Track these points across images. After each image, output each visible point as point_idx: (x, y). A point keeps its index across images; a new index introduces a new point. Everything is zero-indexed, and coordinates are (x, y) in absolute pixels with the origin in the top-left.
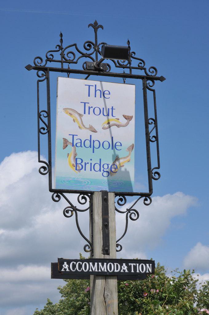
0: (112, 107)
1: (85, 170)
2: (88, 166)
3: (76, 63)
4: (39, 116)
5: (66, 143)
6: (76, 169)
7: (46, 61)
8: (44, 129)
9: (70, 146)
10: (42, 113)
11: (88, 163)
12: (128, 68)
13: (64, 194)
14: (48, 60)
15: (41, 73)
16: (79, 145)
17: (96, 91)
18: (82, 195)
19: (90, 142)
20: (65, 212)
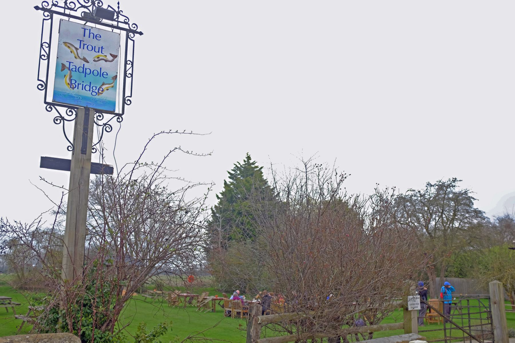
0: (102, 47)
1: (78, 88)
2: (80, 86)
3: (76, 11)
4: (42, 45)
5: (64, 67)
6: (71, 87)
7: (52, 5)
8: (45, 56)
9: (66, 70)
10: (44, 44)
11: (80, 84)
12: (116, 21)
13: (56, 107)
14: (54, 5)
15: (46, 14)
16: (74, 70)
17: (90, 34)
18: (70, 109)
19: (83, 68)
20: (55, 120)
